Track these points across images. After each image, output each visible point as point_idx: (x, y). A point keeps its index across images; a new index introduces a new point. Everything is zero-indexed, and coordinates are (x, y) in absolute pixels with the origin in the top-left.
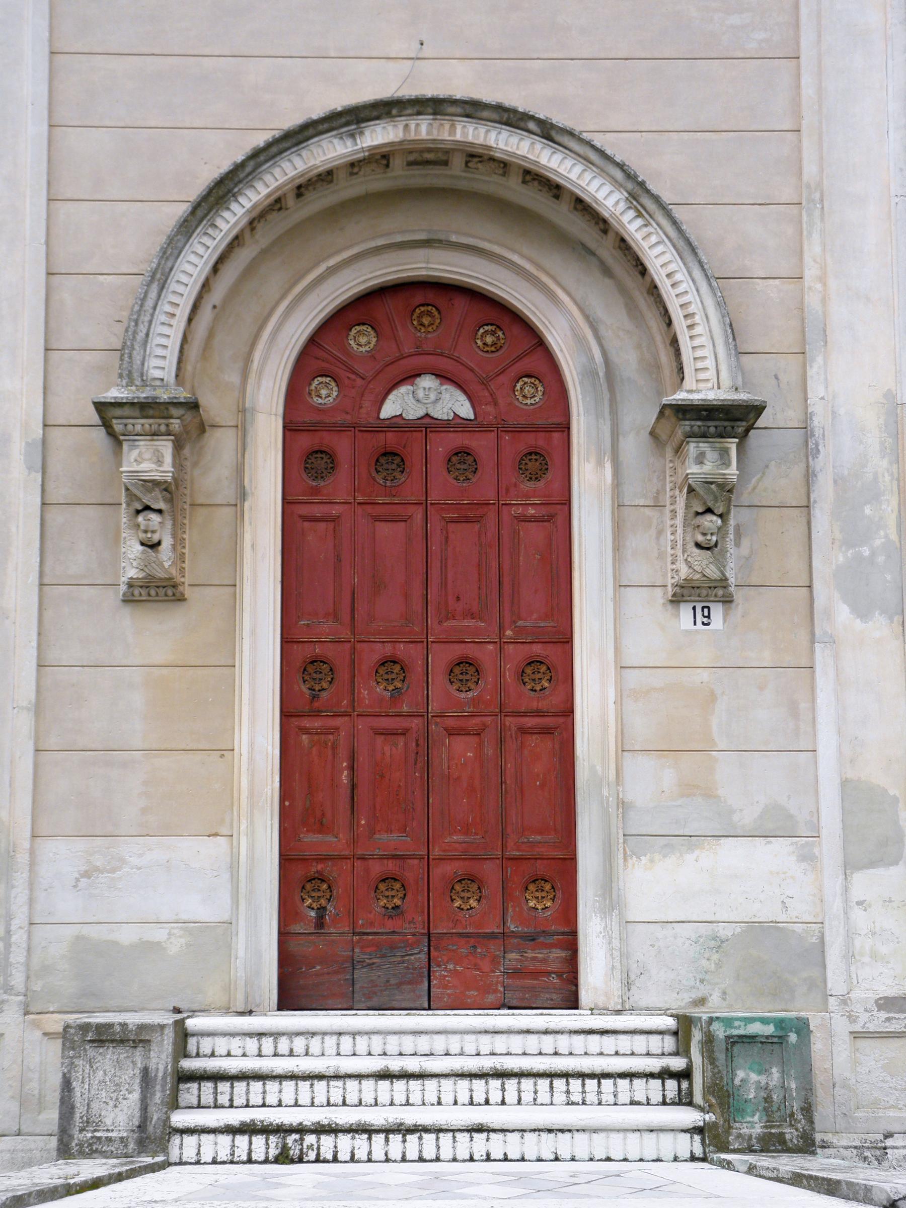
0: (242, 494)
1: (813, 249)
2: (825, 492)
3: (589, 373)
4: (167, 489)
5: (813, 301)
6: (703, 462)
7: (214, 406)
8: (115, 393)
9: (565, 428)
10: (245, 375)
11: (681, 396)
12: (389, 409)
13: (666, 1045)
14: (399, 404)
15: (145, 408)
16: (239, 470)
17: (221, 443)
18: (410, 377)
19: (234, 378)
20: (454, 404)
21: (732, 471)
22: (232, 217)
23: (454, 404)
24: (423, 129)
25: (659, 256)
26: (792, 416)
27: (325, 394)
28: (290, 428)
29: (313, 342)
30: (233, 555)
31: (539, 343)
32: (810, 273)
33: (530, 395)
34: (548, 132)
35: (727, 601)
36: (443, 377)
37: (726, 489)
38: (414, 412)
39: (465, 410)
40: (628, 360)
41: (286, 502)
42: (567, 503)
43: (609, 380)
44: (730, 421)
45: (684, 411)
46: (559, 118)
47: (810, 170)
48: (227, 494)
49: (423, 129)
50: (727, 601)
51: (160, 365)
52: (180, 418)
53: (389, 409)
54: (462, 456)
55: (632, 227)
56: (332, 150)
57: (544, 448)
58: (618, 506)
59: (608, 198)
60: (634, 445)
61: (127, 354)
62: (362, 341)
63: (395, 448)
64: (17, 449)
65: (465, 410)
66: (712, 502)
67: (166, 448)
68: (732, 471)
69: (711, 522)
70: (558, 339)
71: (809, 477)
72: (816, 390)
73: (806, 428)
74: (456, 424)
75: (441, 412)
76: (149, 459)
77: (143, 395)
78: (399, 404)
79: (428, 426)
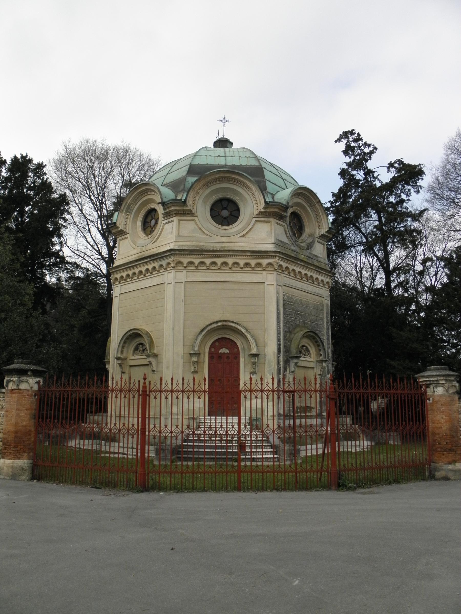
0: (204, 362)
1: (266, 335)
2: (267, 362)
3: (242, 349)
4: (197, 362)
5: (266, 341)
6: (253, 360)
7: (201, 352)
8: (192, 352)
9: (239, 354)
10: (205, 348)
11: (251, 353)
12: (220, 352)
13: (98, 448)
14: (221, 351)
15: (195, 354)
16: (204, 359)
17: (202, 356)
18: (222, 348)
19: (203, 348)
20: (227, 351)
21: (256, 361)
22: (204, 333)
23: (227, 351)
24: (224, 323)
25: (249, 337)
26: (264, 353)
27: (213, 350)
28: (209, 354)
29: (212, 344)
30: (203, 368)
31: (236, 344)
32: (266, 338)
33: (235, 350)
34: (237, 324)
35: (256, 374)
36: (226, 348)
37: (255, 363)
38: (223, 352)
39: (228, 352)
40: (246, 347)
41: (209, 362)
42: (239, 362)
43: (244, 349)
44: (256, 356)
45: (251, 354)
46: (239, 323)
47: (266, 326)
48: (202, 361)
49: (224, 323)
50: (256, 374)
51: (196, 349)
52: (198, 354)
53: (220, 352)
54: (228, 357)
55: (246, 334)
56: (214, 325)
57: (237, 357)
58: (245, 363)
59: (244, 331)
60: (246, 356)
61: (193, 346)
62: (217, 344)
63: (220, 356)
64: (180, 356)
65: (228, 352)
66: (254, 363)
67: (197, 358)
68: (256, 361)
69: (254, 366)
70: (238, 344)
71: (265, 360)
72: (266, 351)
73: (265, 355)
74: (227, 353)
75: (226, 352)
76: (195, 359)
77: (195, 352)
78: (221, 351)
79: (224, 354)
